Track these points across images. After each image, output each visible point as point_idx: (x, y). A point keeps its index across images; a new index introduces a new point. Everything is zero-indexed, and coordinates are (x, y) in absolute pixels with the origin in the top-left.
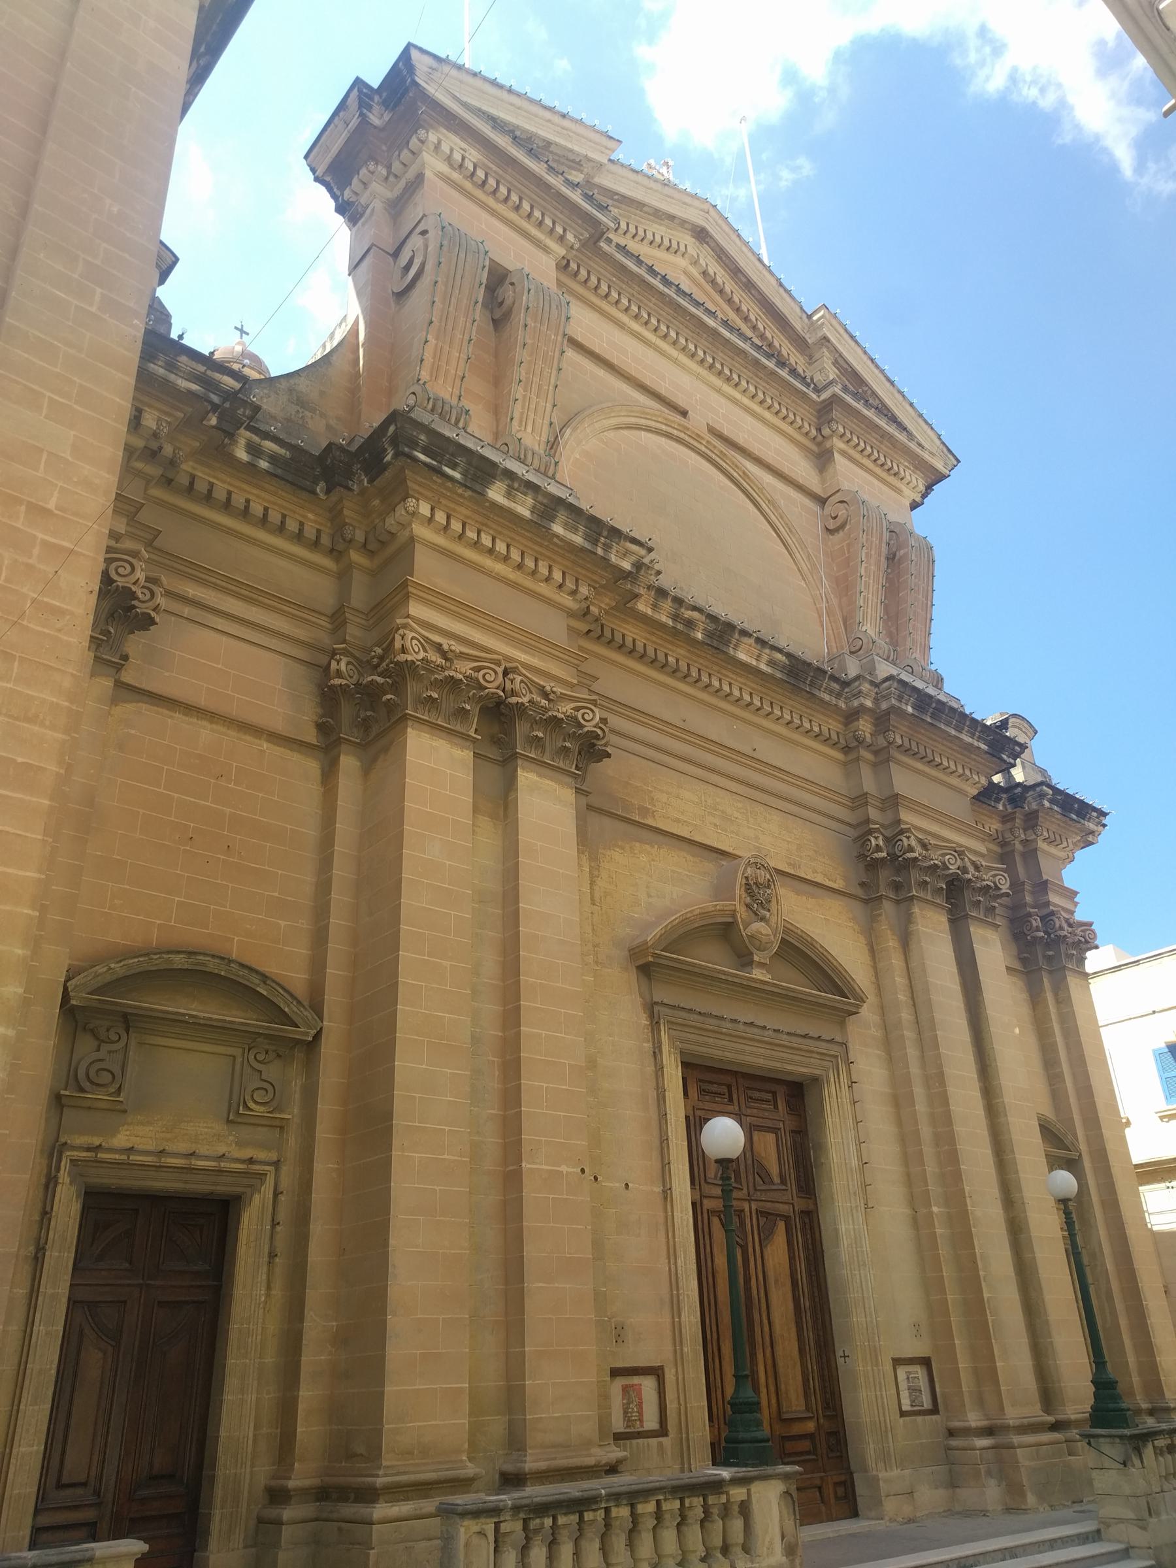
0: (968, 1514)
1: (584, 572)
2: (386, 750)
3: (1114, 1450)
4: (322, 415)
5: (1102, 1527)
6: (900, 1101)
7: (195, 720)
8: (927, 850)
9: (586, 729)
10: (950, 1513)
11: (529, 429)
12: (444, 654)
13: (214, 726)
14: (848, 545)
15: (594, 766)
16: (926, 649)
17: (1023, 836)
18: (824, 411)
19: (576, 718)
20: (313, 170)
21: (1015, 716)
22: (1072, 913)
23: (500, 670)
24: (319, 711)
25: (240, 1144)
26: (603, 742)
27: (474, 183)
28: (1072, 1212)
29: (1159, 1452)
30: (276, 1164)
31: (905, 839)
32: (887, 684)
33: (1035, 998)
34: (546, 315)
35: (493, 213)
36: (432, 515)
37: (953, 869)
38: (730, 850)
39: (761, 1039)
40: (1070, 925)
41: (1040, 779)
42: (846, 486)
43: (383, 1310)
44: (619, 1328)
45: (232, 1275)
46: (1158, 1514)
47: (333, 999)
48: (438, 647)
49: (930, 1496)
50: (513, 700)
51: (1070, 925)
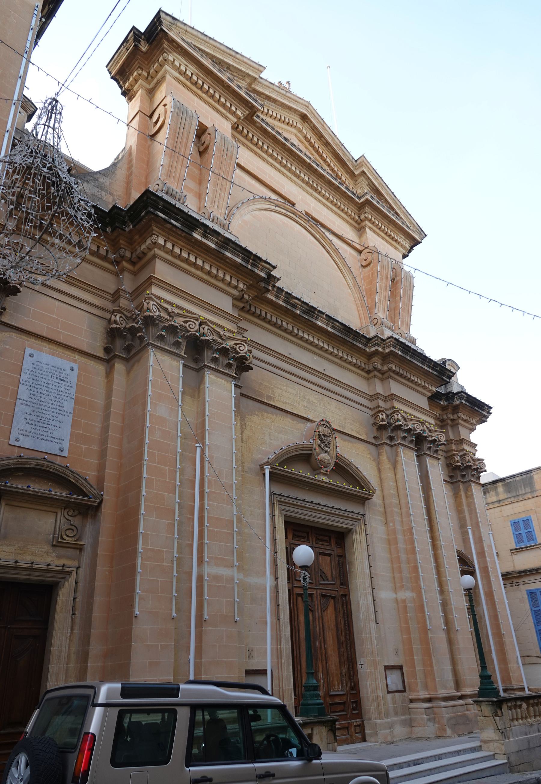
0: (418, 739)
1: (241, 277)
2: (138, 361)
3: (487, 709)
4: (111, 194)
5: (482, 744)
6: (391, 542)
7: (40, 343)
8: (406, 421)
9: (240, 354)
10: (409, 739)
11: (216, 207)
12: (169, 314)
13: (51, 346)
14: (372, 274)
15: (244, 374)
16: (408, 325)
17: (452, 417)
18: (361, 207)
19: (235, 349)
20: (110, 73)
21: (450, 360)
22: (474, 454)
23: (198, 323)
24: (106, 341)
25: (59, 557)
26: (249, 362)
27: (191, 82)
28: (471, 594)
29: (510, 708)
30: (78, 568)
31: (396, 416)
32: (389, 340)
33: (456, 495)
34: (225, 150)
35: (201, 98)
36: (165, 244)
37: (418, 431)
38: (311, 418)
39: (322, 510)
40: (473, 460)
41: (460, 390)
42: (371, 244)
43: (130, 640)
44: (250, 650)
45: (53, 623)
46: (509, 738)
47: (109, 485)
48: (166, 310)
49: (399, 731)
50: (203, 338)
51: (473, 460)
